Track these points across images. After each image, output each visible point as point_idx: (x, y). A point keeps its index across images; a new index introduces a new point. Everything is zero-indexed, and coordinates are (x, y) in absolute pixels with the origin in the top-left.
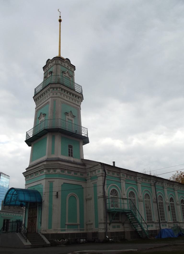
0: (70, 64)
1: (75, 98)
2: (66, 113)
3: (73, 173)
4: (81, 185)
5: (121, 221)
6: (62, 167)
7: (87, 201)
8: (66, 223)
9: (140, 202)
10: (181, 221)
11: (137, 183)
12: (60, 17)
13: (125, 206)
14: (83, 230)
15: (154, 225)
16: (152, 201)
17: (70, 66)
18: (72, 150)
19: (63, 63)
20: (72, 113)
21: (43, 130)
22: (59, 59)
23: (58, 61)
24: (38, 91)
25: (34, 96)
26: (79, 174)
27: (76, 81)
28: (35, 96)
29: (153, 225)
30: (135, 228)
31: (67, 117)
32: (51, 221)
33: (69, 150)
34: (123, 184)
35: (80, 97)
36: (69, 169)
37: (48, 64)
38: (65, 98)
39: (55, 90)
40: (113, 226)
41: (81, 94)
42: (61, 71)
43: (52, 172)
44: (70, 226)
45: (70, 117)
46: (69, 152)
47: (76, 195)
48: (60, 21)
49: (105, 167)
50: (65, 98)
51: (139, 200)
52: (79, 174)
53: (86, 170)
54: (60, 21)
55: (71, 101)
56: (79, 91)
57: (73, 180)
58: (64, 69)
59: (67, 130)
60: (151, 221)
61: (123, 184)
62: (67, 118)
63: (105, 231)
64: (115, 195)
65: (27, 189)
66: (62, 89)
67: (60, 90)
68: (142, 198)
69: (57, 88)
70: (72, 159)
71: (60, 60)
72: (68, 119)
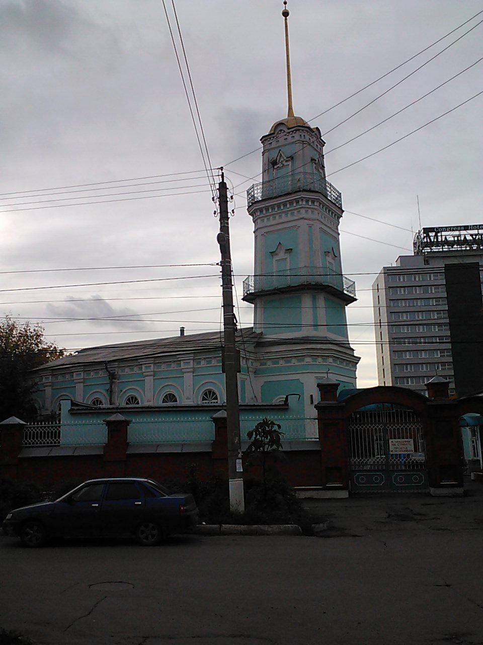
12: (285, 3)
48: (286, 14)
54: (286, 14)
67: (304, 203)
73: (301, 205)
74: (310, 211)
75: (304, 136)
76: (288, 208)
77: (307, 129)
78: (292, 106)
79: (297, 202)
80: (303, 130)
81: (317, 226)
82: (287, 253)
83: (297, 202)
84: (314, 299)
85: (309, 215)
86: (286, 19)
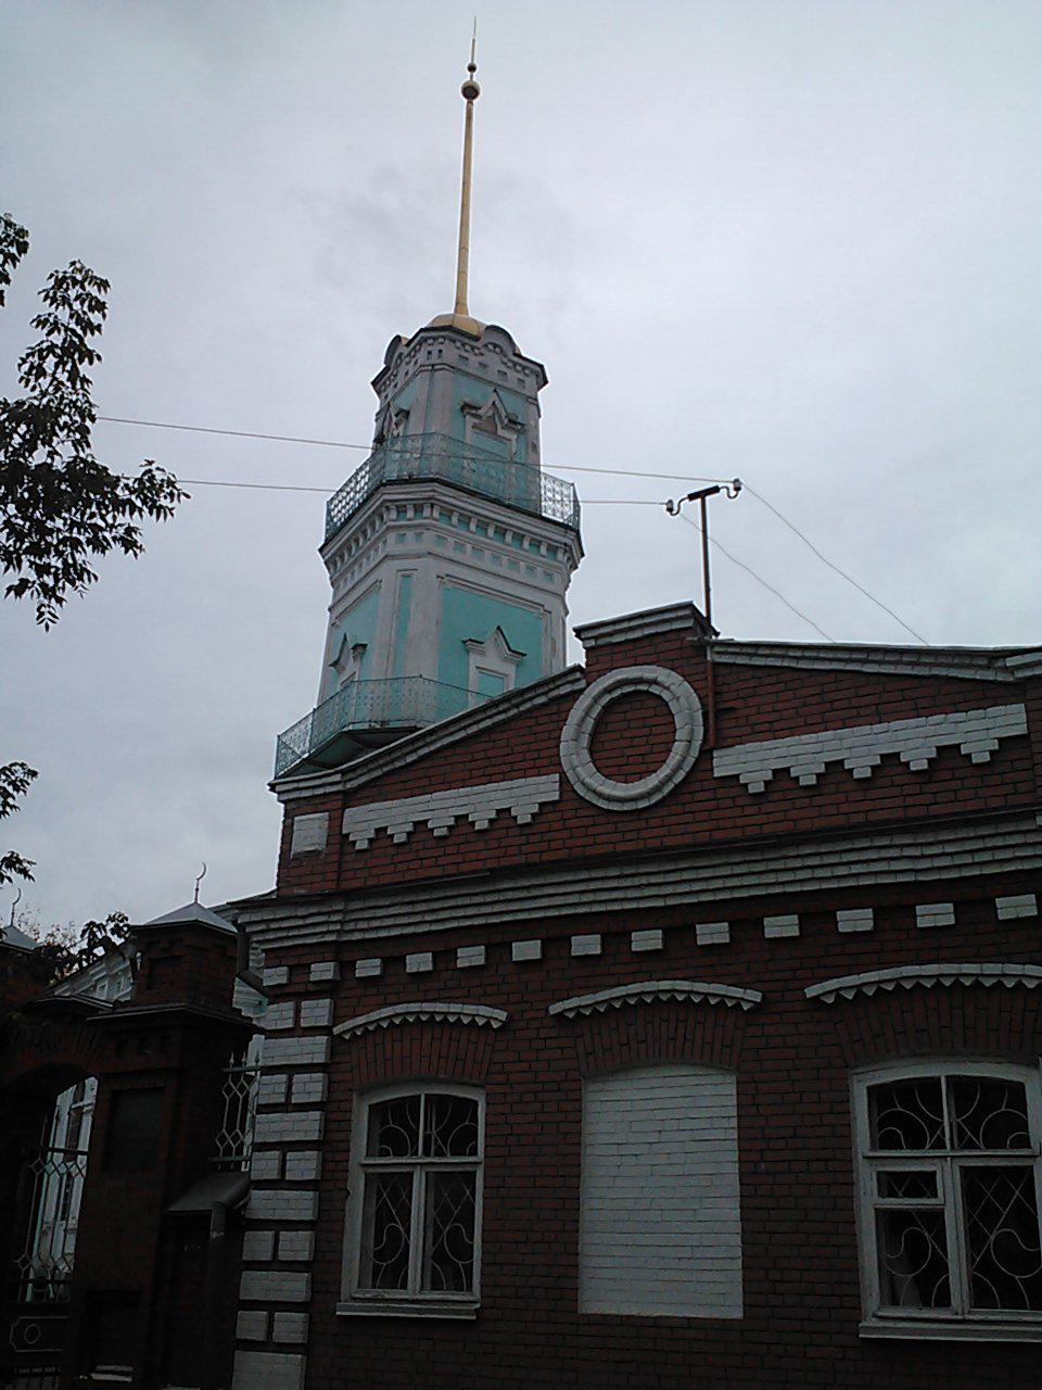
6: (288, 938)
12: (472, 68)
21: (334, 741)
22: (444, 332)
24: (339, 516)
25: (322, 542)
27: (548, 458)
28: (327, 542)
31: (474, 660)
37: (397, 366)
38: (468, 556)
39: (410, 514)
40: (1029, 1146)
41: (571, 529)
48: (471, 92)
54: (471, 92)
56: (554, 510)
62: (473, 672)
67: (436, 514)
69: (422, 506)
74: (410, 534)
75: (440, 351)
76: (410, 520)
77: (421, 335)
78: (465, 299)
79: (418, 509)
80: (435, 339)
81: (429, 569)
82: (512, 662)
83: (418, 509)
85: (411, 544)
86: (470, 103)
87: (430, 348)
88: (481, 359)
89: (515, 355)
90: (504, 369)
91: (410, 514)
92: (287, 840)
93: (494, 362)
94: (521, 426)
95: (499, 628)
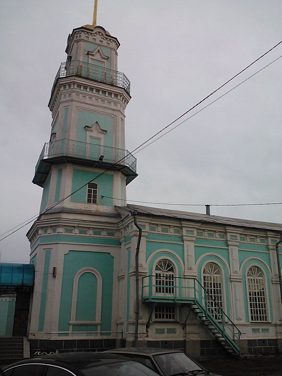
0: (105, 36)
1: (90, 93)
2: (86, 126)
3: (91, 232)
4: (110, 253)
5: (178, 321)
7: (119, 281)
8: (70, 322)
9: (232, 283)
10: (240, 319)
11: (228, 246)
13: (188, 290)
14: (109, 334)
15: (272, 329)
16: (270, 280)
17: (107, 39)
18: (95, 192)
19: (90, 36)
20: (98, 124)
23: (80, 35)
26: (104, 234)
29: (174, 329)
30: (214, 333)
31: (88, 133)
32: (50, 319)
33: (90, 191)
34: (235, 252)
35: (124, 95)
36: (80, 226)
38: (88, 101)
39: (67, 88)
40: (157, 329)
42: (85, 51)
43: (50, 233)
44: (77, 327)
45: (95, 134)
46: (89, 196)
47: (96, 270)
49: (137, 218)
50: (88, 101)
51: (230, 278)
52: (104, 234)
53: (118, 225)
55: (106, 105)
57: (101, 246)
58: (91, 47)
59: (87, 158)
60: (263, 321)
61: (190, 247)
62: (88, 137)
63: (134, 338)
64: (169, 270)
65: (29, 263)
66: (79, 86)
67: (76, 87)
68: (240, 273)
70: (93, 208)
71: (84, 32)
72: (91, 137)
73: (72, 89)
84: (60, 171)
87: (77, 35)
88: (93, 37)
89: (106, 35)
90: (102, 40)
91: (67, 88)
92: (236, 226)
93: (98, 38)
94: (110, 59)
95: (97, 122)
